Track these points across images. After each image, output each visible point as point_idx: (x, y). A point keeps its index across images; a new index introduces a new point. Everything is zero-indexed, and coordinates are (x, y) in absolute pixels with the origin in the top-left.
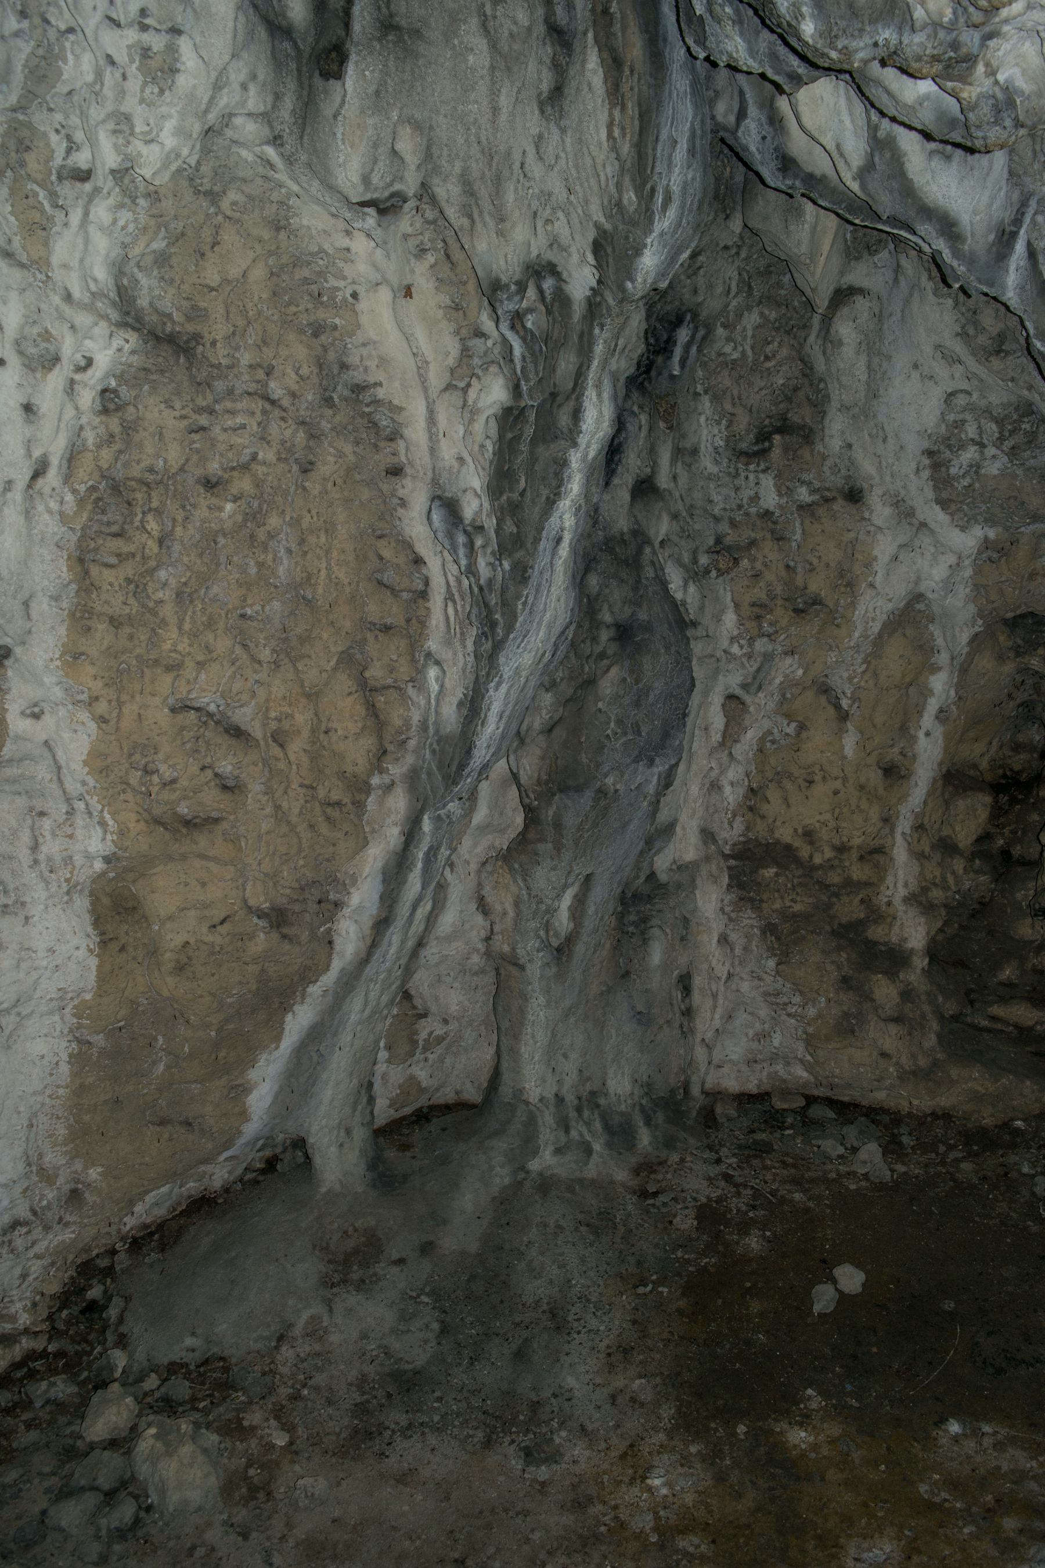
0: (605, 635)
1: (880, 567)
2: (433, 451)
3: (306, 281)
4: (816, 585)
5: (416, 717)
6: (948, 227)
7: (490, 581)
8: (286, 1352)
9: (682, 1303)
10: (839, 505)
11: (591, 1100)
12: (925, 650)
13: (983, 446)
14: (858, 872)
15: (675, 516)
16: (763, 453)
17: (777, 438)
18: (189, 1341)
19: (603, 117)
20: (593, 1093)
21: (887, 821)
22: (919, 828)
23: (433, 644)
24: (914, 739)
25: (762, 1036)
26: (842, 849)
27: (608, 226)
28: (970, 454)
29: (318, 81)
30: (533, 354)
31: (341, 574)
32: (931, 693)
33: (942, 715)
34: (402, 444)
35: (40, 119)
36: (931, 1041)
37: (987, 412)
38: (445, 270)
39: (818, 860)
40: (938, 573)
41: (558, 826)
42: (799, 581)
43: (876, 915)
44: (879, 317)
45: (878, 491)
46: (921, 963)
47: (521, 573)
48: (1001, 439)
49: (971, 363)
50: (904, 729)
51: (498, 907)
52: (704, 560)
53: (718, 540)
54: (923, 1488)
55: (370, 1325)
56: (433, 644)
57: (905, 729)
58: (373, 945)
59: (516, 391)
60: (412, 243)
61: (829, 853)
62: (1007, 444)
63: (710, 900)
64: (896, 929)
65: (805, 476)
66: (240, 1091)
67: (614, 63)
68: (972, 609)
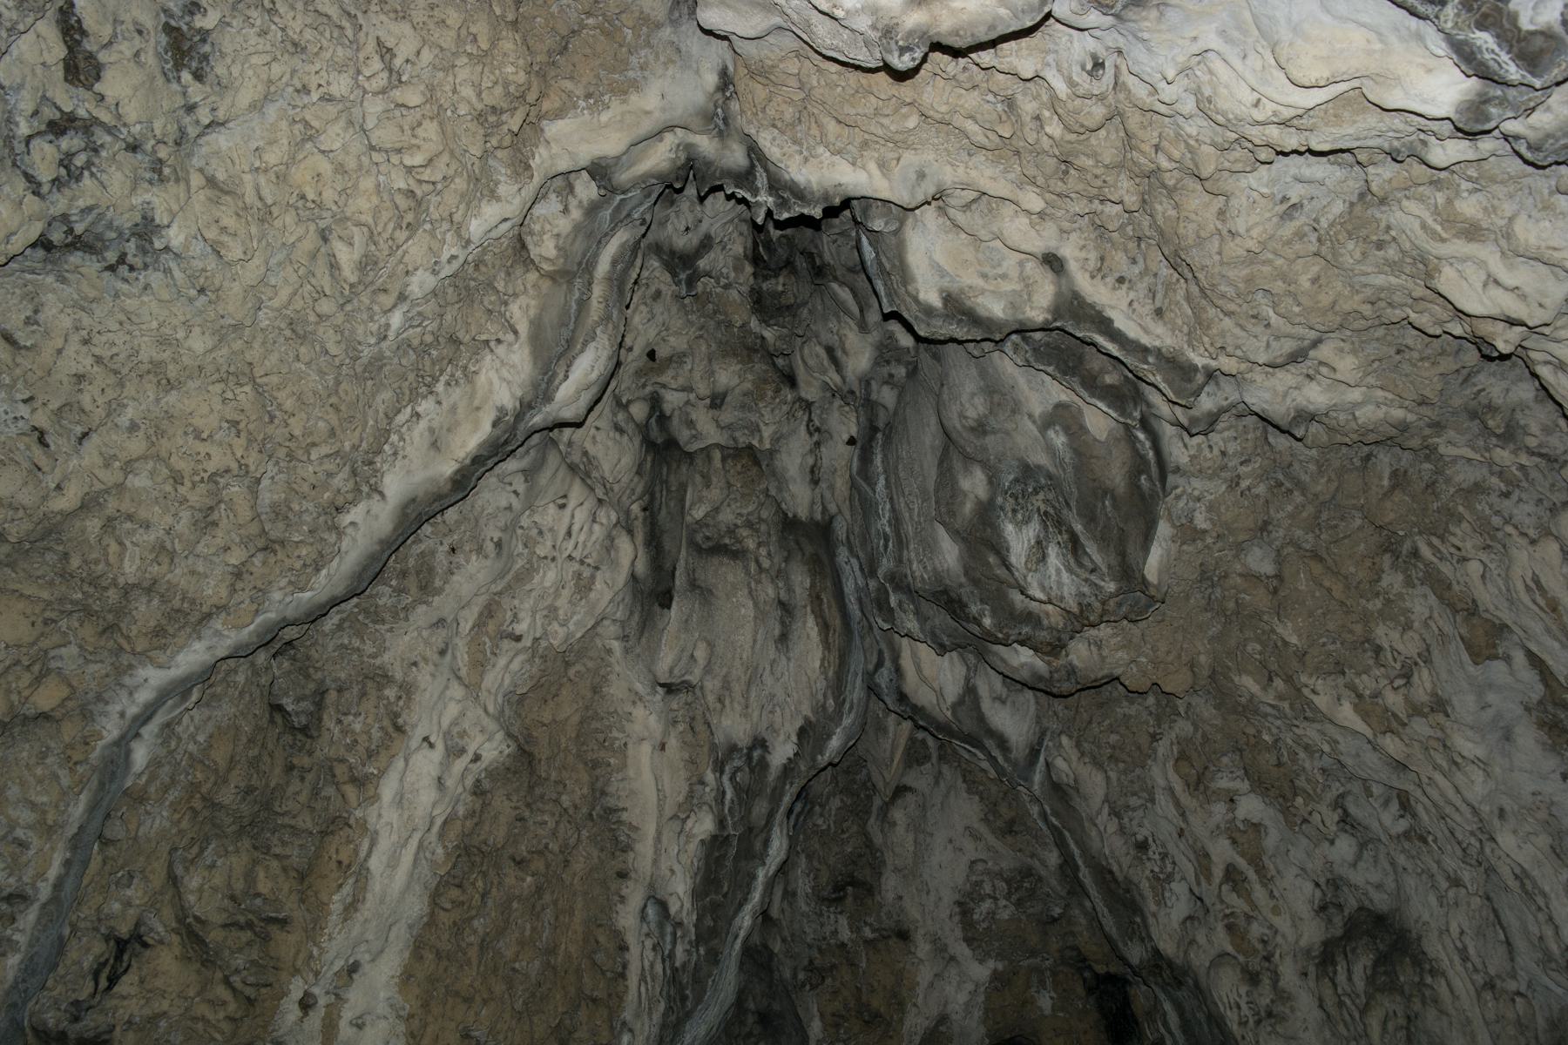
0: (751, 1019)
1: (920, 990)
2: (655, 862)
3: (597, 730)
4: (877, 1003)
6: (1002, 743)
7: (684, 965)
13: (996, 899)
15: (784, 940)
16: (840, 900)
17: (850, 889)
19: (819, 654)
23: (627, 1015)
27: (813, 719)
28: (987, 905)
29: (657, 608)
30: (739, 799)
31: (572, 949)
34: (631, 855)
35: (506, 602)
37: (1000, 875)
40: (962, 998)
42: (864, 999)
44: (923, 808)
45: (921, 931)
47: (714, 957)
49: (991, 839)
52: (801, 976)
53: (811, 962)
56: (627, 1015)
59: (721, 823)
60: (672, 715)
62: (1014, 898)
65: (869, 920)
67: (825, 627)
68: (982, 1030)
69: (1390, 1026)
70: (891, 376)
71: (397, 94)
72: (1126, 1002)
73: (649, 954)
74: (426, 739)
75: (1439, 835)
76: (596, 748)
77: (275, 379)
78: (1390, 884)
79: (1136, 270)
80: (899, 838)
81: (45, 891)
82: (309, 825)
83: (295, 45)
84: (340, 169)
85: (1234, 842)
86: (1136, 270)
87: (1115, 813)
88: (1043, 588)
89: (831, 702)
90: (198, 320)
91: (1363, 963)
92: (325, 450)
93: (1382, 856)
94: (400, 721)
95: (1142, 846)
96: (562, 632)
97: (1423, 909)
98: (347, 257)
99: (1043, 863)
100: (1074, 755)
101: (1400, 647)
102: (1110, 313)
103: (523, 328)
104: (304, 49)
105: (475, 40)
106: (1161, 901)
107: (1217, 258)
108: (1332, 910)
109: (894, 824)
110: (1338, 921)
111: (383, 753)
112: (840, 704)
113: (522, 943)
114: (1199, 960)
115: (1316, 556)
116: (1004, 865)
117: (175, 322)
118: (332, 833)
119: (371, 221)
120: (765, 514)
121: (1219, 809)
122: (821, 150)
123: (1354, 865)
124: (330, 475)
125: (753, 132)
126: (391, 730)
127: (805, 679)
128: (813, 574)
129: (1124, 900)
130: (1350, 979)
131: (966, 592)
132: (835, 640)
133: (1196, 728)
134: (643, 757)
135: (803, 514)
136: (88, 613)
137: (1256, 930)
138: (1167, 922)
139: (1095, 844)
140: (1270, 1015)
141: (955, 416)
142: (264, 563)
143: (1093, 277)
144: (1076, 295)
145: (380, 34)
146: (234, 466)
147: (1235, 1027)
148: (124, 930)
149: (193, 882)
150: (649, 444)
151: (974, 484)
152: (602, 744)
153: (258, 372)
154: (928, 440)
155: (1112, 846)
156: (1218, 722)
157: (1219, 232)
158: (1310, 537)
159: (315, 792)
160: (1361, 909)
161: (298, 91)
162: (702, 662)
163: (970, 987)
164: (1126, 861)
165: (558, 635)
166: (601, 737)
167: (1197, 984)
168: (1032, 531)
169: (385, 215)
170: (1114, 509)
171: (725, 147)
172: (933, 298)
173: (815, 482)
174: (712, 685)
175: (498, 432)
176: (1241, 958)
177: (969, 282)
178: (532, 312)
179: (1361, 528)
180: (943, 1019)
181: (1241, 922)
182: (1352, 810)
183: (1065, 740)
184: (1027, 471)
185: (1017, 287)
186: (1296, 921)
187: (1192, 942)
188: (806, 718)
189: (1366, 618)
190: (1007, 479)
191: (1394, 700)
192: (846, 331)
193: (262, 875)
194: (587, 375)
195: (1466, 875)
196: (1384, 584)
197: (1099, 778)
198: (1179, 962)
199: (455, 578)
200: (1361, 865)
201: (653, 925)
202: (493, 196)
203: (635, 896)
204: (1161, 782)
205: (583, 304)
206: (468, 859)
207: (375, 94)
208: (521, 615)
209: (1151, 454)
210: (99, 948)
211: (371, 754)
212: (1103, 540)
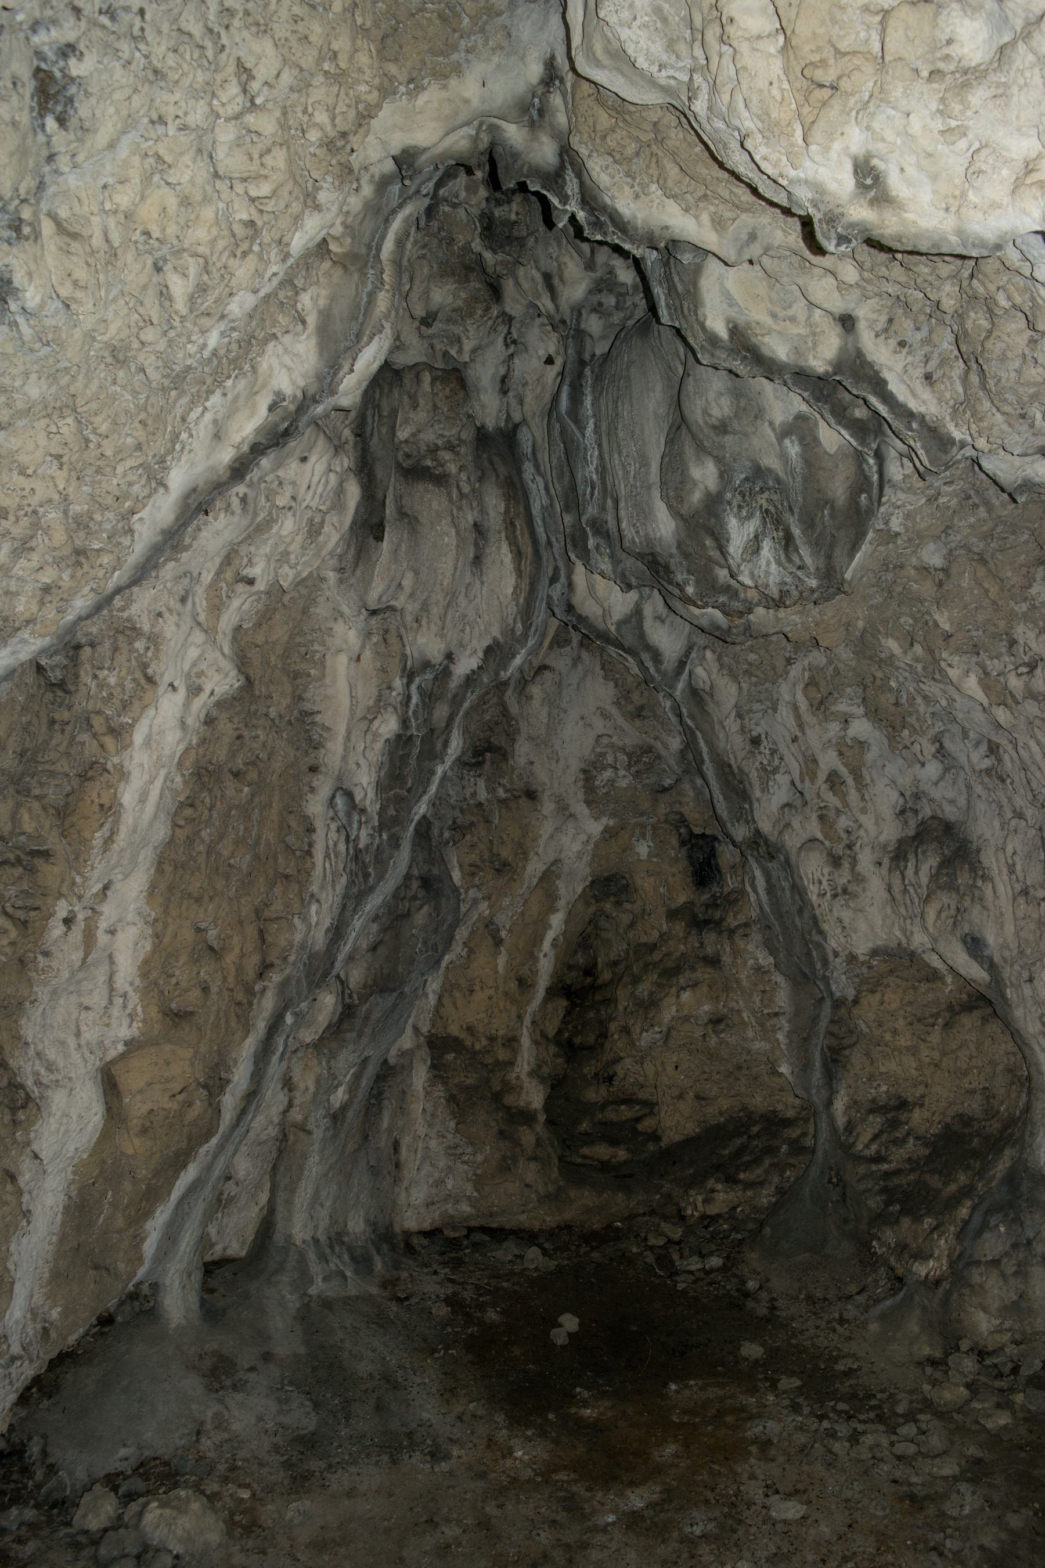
1: (542, 842)
2: (344, 758)
3: (299, 644)
4: (506, 853)
5: (298, 937)
6: (657, 656)
7: (367, 847)
8: (206, 1443)
9: (470, 1357)
10: (523, 801)
11: (337, 1238)
14: (502, 1054)
16: (479, 764)
17: (488, 755)
18: (123, 1452)
20: (338, 1234)
21: (520, 1017)
22: (533, 1022)
23: (314, 888)
24: (536, 960)
25: (440, 1183)
26: (492, 1039)
28: (608, 774)
29: (371, 541)
32: (550, 927)
33: (554, 944)
35: (244, 550)
36: (555, 1173)
37: (623, 749)
38: (382, 648)
39: (477, 1047)
40: (576, 847)
41: (367, 1018)
43: (508, 1087)
44: (559, 685)
45: (548, 793)
46: (542, 1118)
48: (629, 766)
49: (621, 721)
51: (302, 1086)
52: (447, 834)
54: (675, 1419)
55: (253, 1416)
56: (314, 888)
57: (532, 957)
59: (405, 723)
61: (484, 1042)
62: (633, 769)
63: (420, 1076)
64: (524, 1096)
65: (504, 781)
66: (138, 1240)
67: (518, 555)
68: (588, 870)
69: (944, 915)
70: (600, 304)
71: (250, 119)
72: (713, 854)
73: (333, 835)
74: (171, 685)
75: (1017, 779)
77: (94, 406)
78: (962, 801)
79: (919, 336)
80: (535, 712)
82: (66, 769)
83: (156, 72)
84: (185, 202)
85: (841, 754)
86: (919, 336)
87: (740, 716)
88: (752, 575)
89: (519, 625)
90: (36, 367)
91: (930, 864)
92: (130, 463)
93: (960, 780)
94: (150, 671)
95: (756, 742)
96: (291, 573)
97: (985, 829)
98: (179, 288)
99: (666, 746)
100: (715, 667)
101: (1033, 645)
102: (886, 374)
103: (312, 320)
104: (164, 77)
105: (335, 56)
107: (1013, 374)
108: (909, 814)
109: (530, 698)
110: (913, 823)
111: (137, 704)
112: (527, 628)
113: (237, 843)
114: (792, 841)
115: (983, 561)
116: (628, 741)
117: (15, 372)
118: (91, 779)
119: (208, 252)
120: (464, 436)
121: (834, 727)
122: (654, 187)
123: (936, 784)
124: (130, 484)
125: (583, 151)
126: (143, 681)
127: (496, 603)
129: (738, 790)
130: (916, 873)
132: (527, 567)
133: (830, 662)
134: (341, 665)
135: (490, 424)
137: (843, 822)
138: (768, 808)
139: (722, 745)
140: (845, 891)
141: (699, 412)
142: (72, 577)
143: (877, 336)
144: (860, 354)
145: (242, 54)
146: (56, 497)
147: (814, 898)
151: (704, 475)
152: (304, 657)
153: (80, 402)
154: (651, 406)
155: (732, 741)
156: (853, 664)
157: (1024, 356)
158: (982, 545)
160: (933, 817)
161: (153, 122)
162: (408, 590)
163: (583, 837)
164: (740, 755)
166: (303, 650)
167: (787, 861)
168: (752, 526)
169: (221, 244)
170: (831, 521)
171: (534, 138)
172: (720, 328)
173: (504, 392)
174: (411, 608)
175: (275, 417)
176: (827, 843)
177: (757, 317)
178: (322, 302)
179: (1027, 542)
180: (556, 862)
181: (832, 814)
182: (947, 744)
183: (709, 654)
184: (759, 472)
185: (802, 331)
186: (879, 820)
187: (788, 825)
188: (495, 639)
190: (738, 478)
191: (1015, 683)
192: (566, 259)
193: (26, 817)
194: (369, 365)
195: (1029, 813)
196: (1033, 591)
197: (733, 689)
198: (773, 839)
199: (204, 534)
200: (942, 784)
201: (341, 814)
203: (325, 790)
204: (787, 697)
206: (203, 776)
207: (228, 120)
208: (255, 560)
209: (876, 477)
211: (125, 705)
212: (816, 545)
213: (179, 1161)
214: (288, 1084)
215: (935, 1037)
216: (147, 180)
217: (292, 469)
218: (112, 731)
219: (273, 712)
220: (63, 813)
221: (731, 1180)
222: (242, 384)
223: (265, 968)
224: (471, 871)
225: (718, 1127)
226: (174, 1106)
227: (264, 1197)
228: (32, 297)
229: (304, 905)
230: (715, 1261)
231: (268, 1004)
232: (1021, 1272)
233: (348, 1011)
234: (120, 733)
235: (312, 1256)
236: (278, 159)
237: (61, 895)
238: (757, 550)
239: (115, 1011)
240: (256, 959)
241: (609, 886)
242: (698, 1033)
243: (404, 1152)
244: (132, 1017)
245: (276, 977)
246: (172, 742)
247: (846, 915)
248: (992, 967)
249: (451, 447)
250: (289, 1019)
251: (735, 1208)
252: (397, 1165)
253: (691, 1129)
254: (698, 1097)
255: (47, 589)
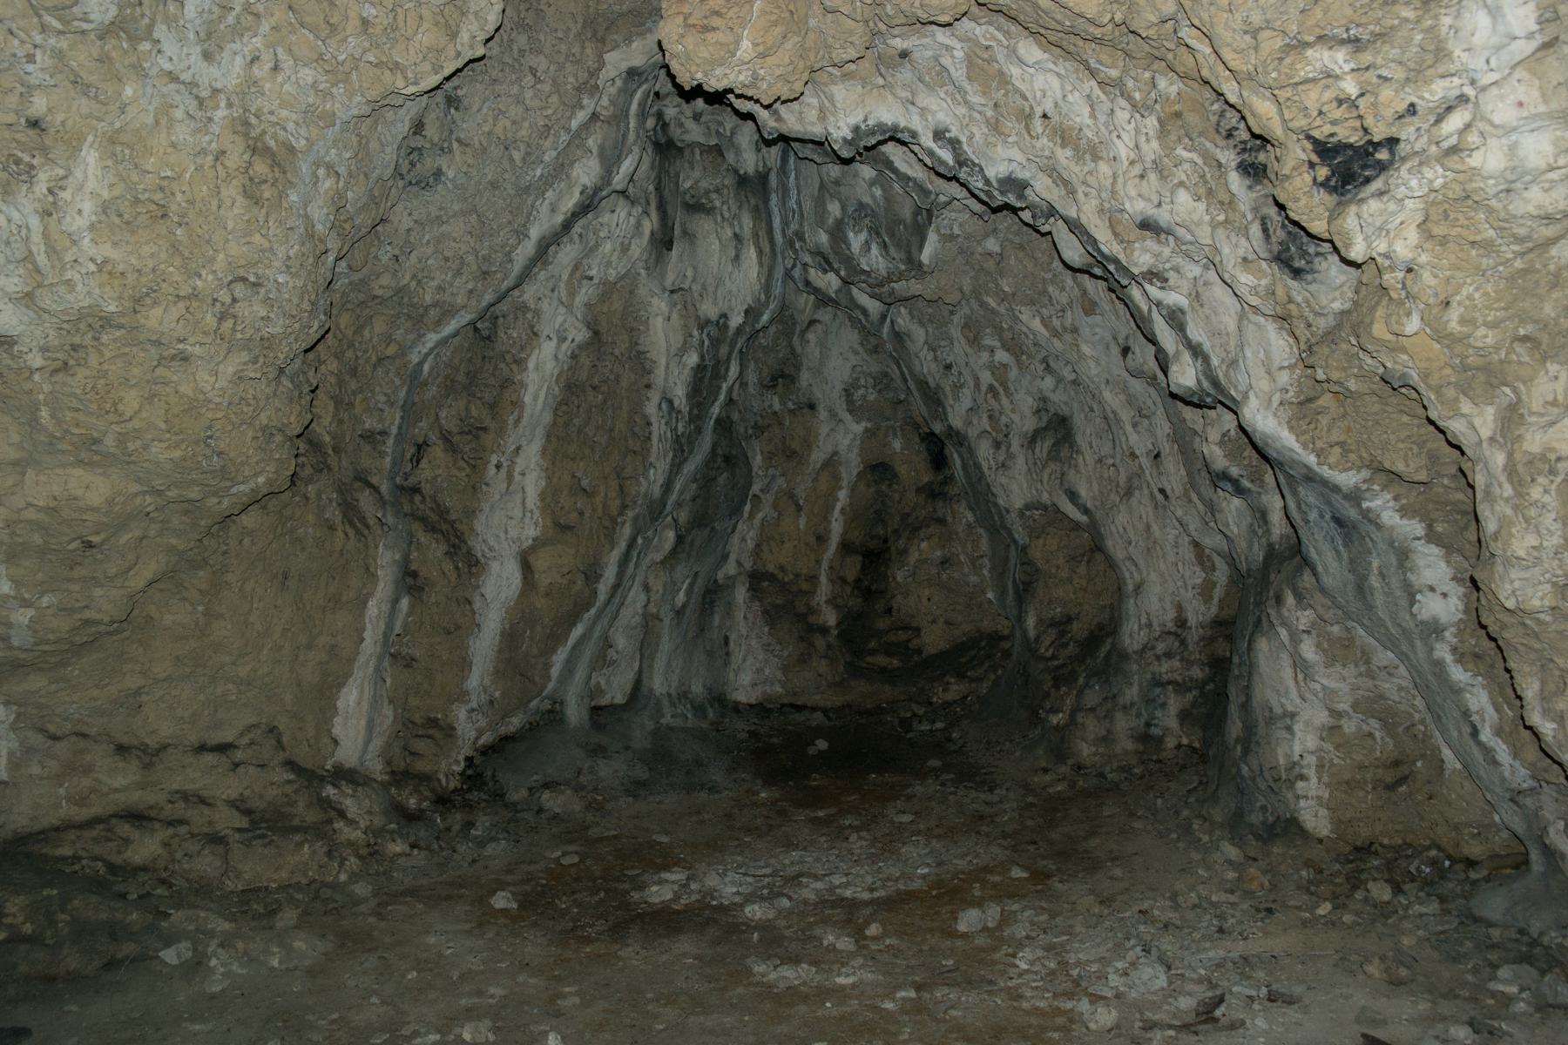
1: (821, 438)
2: (666, 380)
4: (795, 445)
5: (643, 490)
6: (864, 312)
11: (684, 695)
12: (836, 478)
14: (805, 586)
21: (818, 562)
22: (831, 568)
23: (652, 460)
25: (759, 671)
26: (797, 575)
28: (862, 391)
33: (843, 511)
35: (585, 261)
36: (841, 668)
40: (846, 442)
41: (692, 544)
43: (812, 611)
44: (826, 332)
47: (699, 430)
50: (825, 518)
57: (826, 518)
58: (612, 596)
59: (702, 357)
63: (741, 594)
66: (547, 667)
67: (760, 253)
73: (663, 427)
76: (633, 323)
80: (812, 351)
81: (394, 430)
84: (514, 122)
91: (1048, 443)
95: (948, 367)
96: (614, 273)
97: (1078, 420)
98: (517, 156)
100: (908, 318)
103: (595, 151)
106: (957, 398)
110: (1045, 419)
112: (768, 298)
114: (972, 433)
121: (985, 355)
128: (754, 219)
129: (933, 398)
131: (831, 257)
132: (766, 260)
134: (658, 323)
135: (751, 170)
136: (410, 317)
137: (1004, 420)
139: (918, 368)
147: (986, 471)
148: (420, 441)
149: (443, 414)
150: (657, 145)
151: (834, 209)
155: (926, 365)
159: (496, 367)
164: (937, 376)
165: (612, 274)
168: (863, 236)
174: (696, 288)
180: (835, 453)
182: (1052, 364)
184: (861, 206)
186: (1023, 417)
189: (1044, 281)
190: (851, 210)
191: (1056, 322)
202: (582, 107)
203: (655, 397)
205: (625, 136)
206: (571, 389)
210: (413, 450)
211: (522, 348)
212: (898, 246)
213: (573, 618)
214: (647, 588)
215: (1082, 570)
216: (496, 118)
217: (606, 218)
218: (515, 361)
219: (617, 352)
220: (493, 406)
221: (961, 676)
222: (563, 184)
223: (624, 507)
224: (769, 457)
225: (963, 644)
226: (565, 582)
227: (637, 664)
228: (451, 174)
229: (646, 470)
230: (939, 725)
231: (627, 531)
232: (1109, 716)
233: (680, 539)
234: (521, 363)
235: (665, 702)
236: (555, 98)
237: (493, 452)
238: (869, 249)
239: (527, 521)
240: (618, 502)
241: (879, 470)
242: (934, 571)
243: (732, 644)
244: (536, 524)
245: (630, 514)
246: (550, 367)
247: (1004, 480)
248: (1086, 511)
249: (717, 191)
250: (640, 541)
251: (965, 697)
252: (727, 654)
253: (944, 645)
254: (947, 623)
255: (471, 292)
